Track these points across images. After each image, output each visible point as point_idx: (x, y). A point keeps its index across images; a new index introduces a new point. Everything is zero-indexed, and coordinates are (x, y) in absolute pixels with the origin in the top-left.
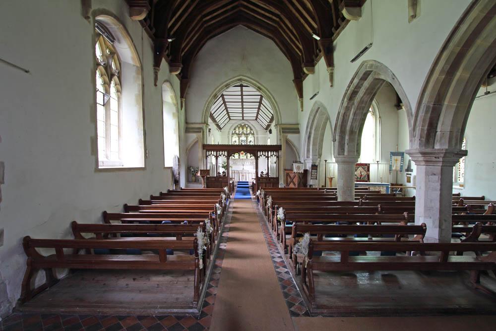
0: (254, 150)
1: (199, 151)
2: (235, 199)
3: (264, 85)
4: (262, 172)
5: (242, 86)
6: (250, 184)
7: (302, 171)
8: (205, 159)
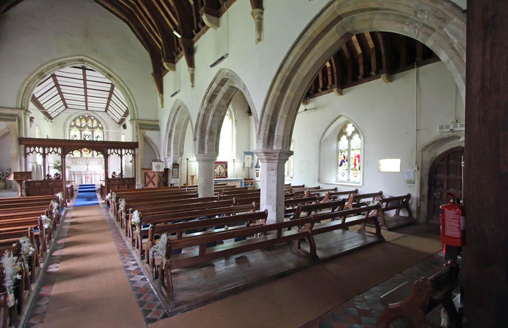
0: (103, 147)
1: (13, 148)
2: (74, 206)
3: (114, 71)
4: (114, 173)
5: (84, 69)
6: (98, 187)
7: (162, 170)
8: (23, 158)
